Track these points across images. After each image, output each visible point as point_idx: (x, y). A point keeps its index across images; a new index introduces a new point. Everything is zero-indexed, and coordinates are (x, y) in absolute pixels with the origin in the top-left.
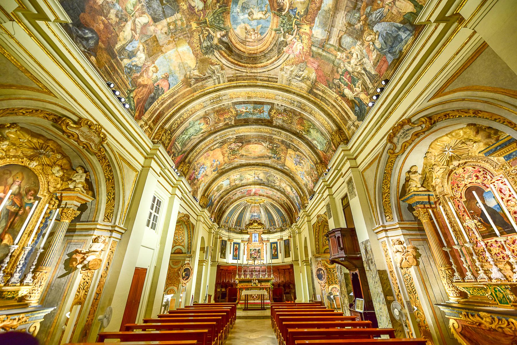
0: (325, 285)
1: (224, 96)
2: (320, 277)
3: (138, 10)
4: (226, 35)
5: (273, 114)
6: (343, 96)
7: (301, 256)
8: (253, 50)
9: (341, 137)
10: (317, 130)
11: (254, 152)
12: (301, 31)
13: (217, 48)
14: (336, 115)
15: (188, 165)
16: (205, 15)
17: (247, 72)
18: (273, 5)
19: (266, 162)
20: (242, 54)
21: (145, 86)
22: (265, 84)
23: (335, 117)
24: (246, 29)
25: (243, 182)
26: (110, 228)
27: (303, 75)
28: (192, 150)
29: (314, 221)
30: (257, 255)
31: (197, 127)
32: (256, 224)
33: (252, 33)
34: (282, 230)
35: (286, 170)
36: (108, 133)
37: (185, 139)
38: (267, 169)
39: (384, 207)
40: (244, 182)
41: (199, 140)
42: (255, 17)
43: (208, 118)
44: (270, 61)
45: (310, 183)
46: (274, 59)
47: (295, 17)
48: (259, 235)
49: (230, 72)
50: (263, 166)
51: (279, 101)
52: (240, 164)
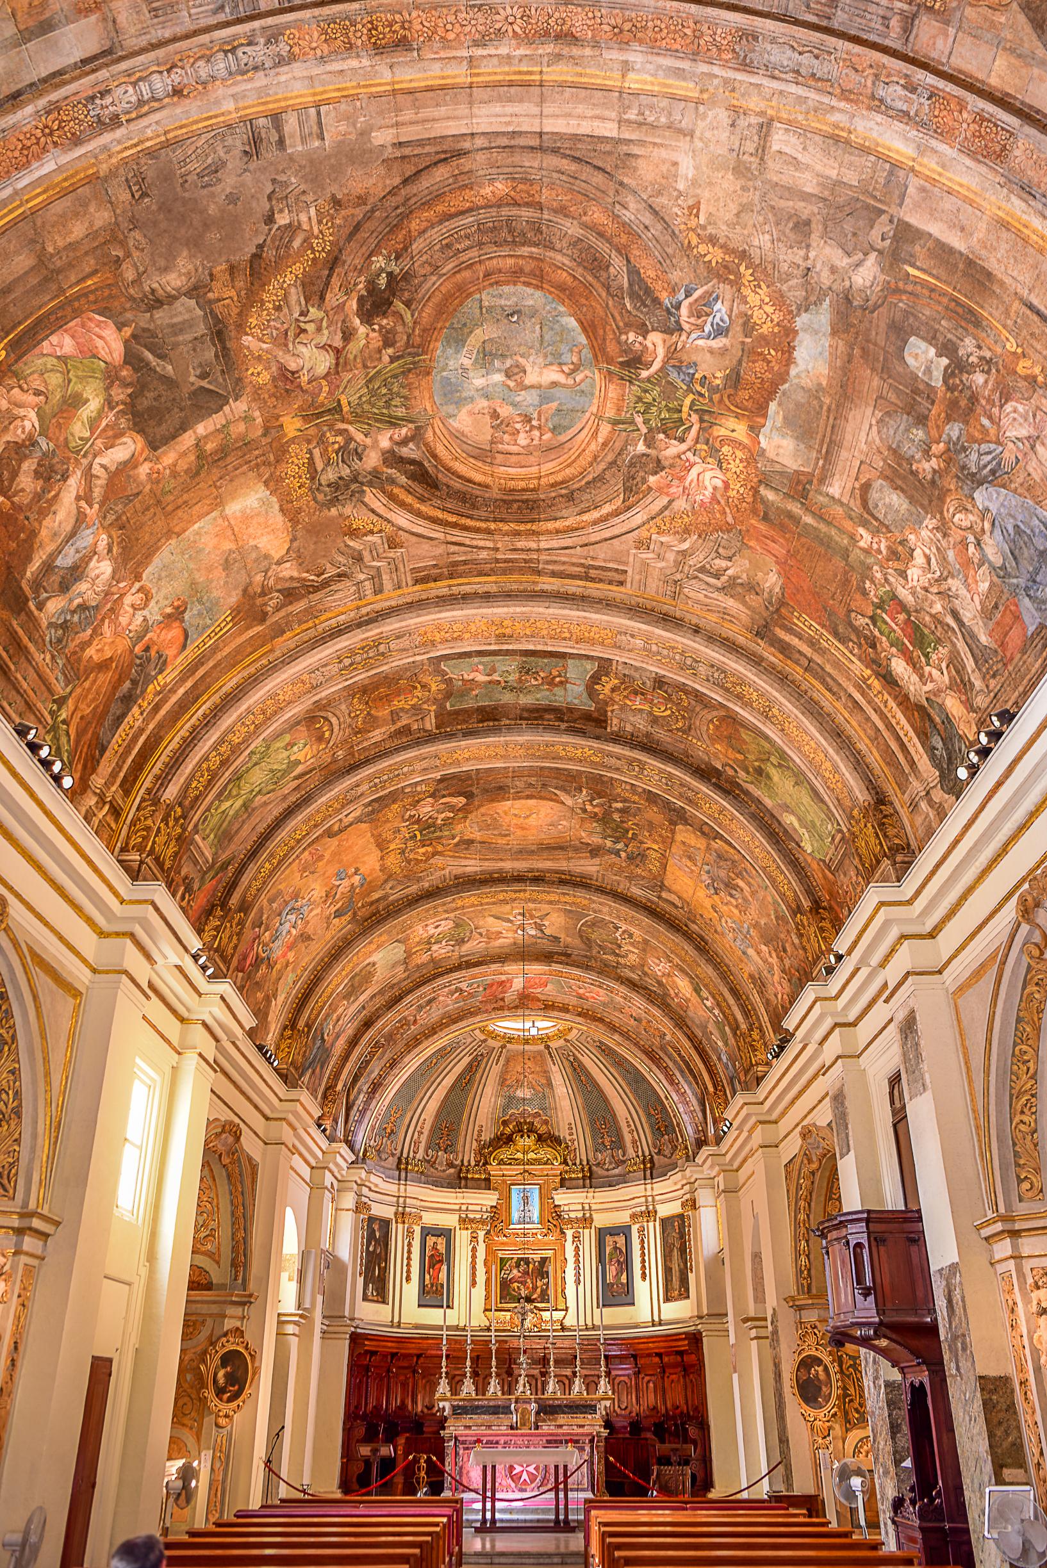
0: (830, 1428)
1: (398, 638)
2: (809, 1392)
3: (104, 430)
4: (417, 436)
5: (607, 691)
6: (889, 680)
7: (739, 1298)
8: (522, 479)
9: (885, 836)
10: (795, 775)
11: (523, 828)
12: (716, 434)
13: (376, 479)
14: (867, 741)
15: (237, 916)
16: (338, 387)
17: (497, 549)
18: (603, 350)
19: (578, 870)
20: (478, 493)
21: (103, 666)
22: (574, 587)
23: (861, 746)
24: (495, 415)
25: (465, 948)
26: (15, 1222)
27: (730, 572)
28: (253, 854)
29: (793, 1146)
30: (535, 1288)
31: (279, 758)
32: (528, 1141)
33: (518, 426)
34: (652, 1170)
35: (668, 908)
36: (18, 896)
37: (231, 813)
38: (581, 897)
39: (1014, 1144)
40: (474, 946)
41: (285, 805)
42: (531, 378)
43: (326, 719)
44: (595, 515)
45: (776, 978)
46: (607, 509)
47: (690, 390)
48: (545, 1197)
49: (426, 555)
50: (562, 882)
51: (631, 655)
52: (456, 877)
